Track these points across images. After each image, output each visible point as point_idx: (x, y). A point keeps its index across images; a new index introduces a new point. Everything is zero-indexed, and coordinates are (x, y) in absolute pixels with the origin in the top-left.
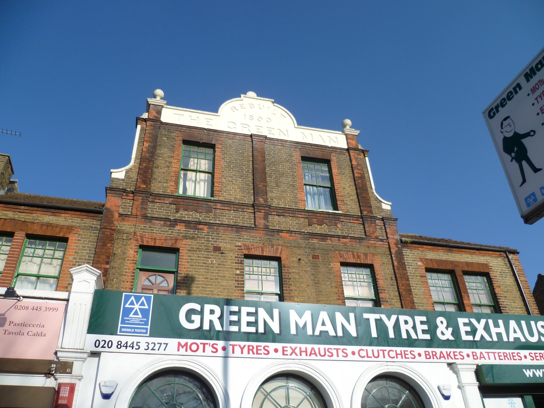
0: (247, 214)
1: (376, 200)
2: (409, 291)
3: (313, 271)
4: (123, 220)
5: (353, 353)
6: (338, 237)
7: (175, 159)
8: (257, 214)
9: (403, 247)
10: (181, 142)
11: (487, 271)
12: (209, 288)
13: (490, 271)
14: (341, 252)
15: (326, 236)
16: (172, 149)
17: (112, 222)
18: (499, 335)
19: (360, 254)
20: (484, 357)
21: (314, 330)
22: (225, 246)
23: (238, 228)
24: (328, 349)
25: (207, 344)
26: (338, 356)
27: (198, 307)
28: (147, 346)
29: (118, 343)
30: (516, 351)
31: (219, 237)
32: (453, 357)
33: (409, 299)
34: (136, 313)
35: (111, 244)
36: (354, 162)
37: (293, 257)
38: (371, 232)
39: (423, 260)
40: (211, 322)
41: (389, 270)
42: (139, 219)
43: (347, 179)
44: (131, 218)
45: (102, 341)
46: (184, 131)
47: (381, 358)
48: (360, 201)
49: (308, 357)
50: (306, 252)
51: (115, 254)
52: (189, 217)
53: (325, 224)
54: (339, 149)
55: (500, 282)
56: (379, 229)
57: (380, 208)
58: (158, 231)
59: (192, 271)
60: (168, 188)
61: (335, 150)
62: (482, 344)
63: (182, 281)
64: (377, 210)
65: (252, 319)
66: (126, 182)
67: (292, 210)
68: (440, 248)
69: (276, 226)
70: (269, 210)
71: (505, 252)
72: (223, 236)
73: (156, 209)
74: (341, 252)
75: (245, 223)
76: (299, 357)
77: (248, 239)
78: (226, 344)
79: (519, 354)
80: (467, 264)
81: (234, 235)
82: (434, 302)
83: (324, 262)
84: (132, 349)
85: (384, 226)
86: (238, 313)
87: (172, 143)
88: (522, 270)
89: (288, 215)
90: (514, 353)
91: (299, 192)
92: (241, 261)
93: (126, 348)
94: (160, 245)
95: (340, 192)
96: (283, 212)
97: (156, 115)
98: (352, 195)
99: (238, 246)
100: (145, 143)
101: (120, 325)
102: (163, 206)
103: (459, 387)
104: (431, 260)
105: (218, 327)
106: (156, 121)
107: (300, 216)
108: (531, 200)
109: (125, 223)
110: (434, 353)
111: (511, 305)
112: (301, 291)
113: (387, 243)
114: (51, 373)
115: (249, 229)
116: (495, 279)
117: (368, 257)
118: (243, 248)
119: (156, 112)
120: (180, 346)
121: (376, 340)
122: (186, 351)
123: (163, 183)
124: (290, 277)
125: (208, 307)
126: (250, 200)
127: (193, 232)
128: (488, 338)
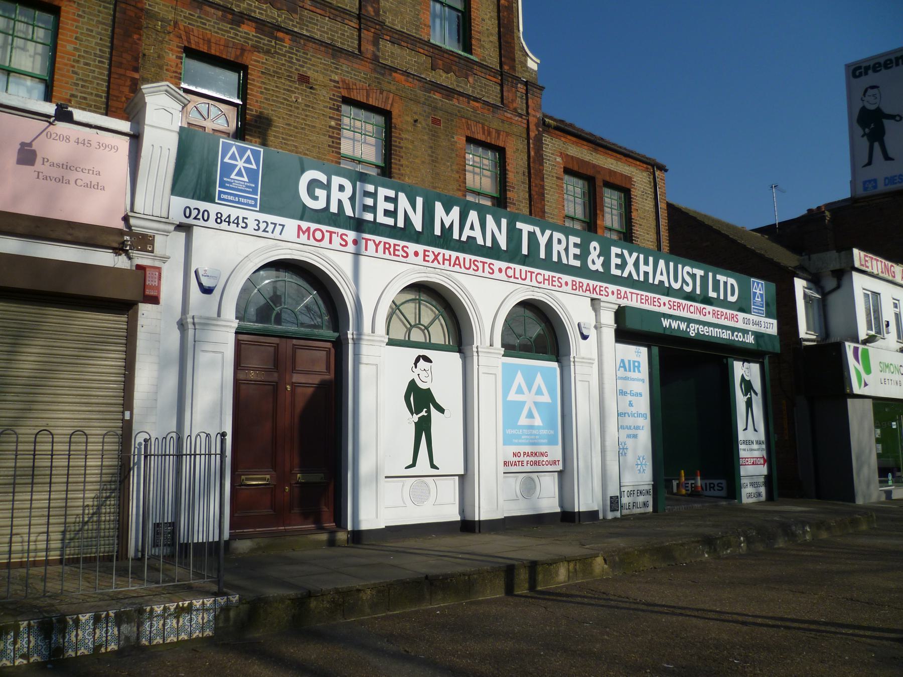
0: (348, 28)
1: (521, 51)
2: (542, 195)
3: (431, 141)
5: (500, 270)
6: (468, 97)
8: (364, 33)
9: (544, 131)
12: (293, 141)
15: (453, 93)
18: (646, 274)
20: (627, 298)
23: (335, 51)
24: (474, 261)
25: (335, 233)
26: (483, 272)
27: (323, 178)
28: (257, 225)
32: (598, 293)
34: (239, 174)
37: (407, 115)
38: (510, 100)
40: (340, 202)
43: (489, 5)
47: (528, 281)
49: (451, 268)
50: (425, 112)
52: (261, 14)
56: (519, 97)
57: (524, 64)
58: (214, 27)
59: (268, 110)
62: (629, 282)
63: (253, 123)
64: (520, 66)
68: (585, 143)
70: (382, 30)
71: (653, 166)
72: (313, 59)
75: (344, 44)
76: (441, 266)
77: (348, 72)
78: (358, 236)
79: (560, 280)
80: (611, 172)
81: (328, 61)
82: (566, 216)
83: (446, 131)
84: (237, 226)
85: (527, 94)
86: (374, 195)
88: (665, 193)
89: (405, 44)
90: (555, 277)
95: (477, 25)
96: (401, 38)
98: (492, 34)
99: (334, 81)
101: (218, 189)
105: (349, 212)
107: (422, 51)
108: (870, 186)
110: (581, 285)
111: (644, 236)
112: (414, 169)
113: (525, 121)
115: (350, 55)
117: (501, 137)
118: (340, 85)
120: (301, 232)
122: (309, 238)
124: (402, 145)
128: (635, 277)
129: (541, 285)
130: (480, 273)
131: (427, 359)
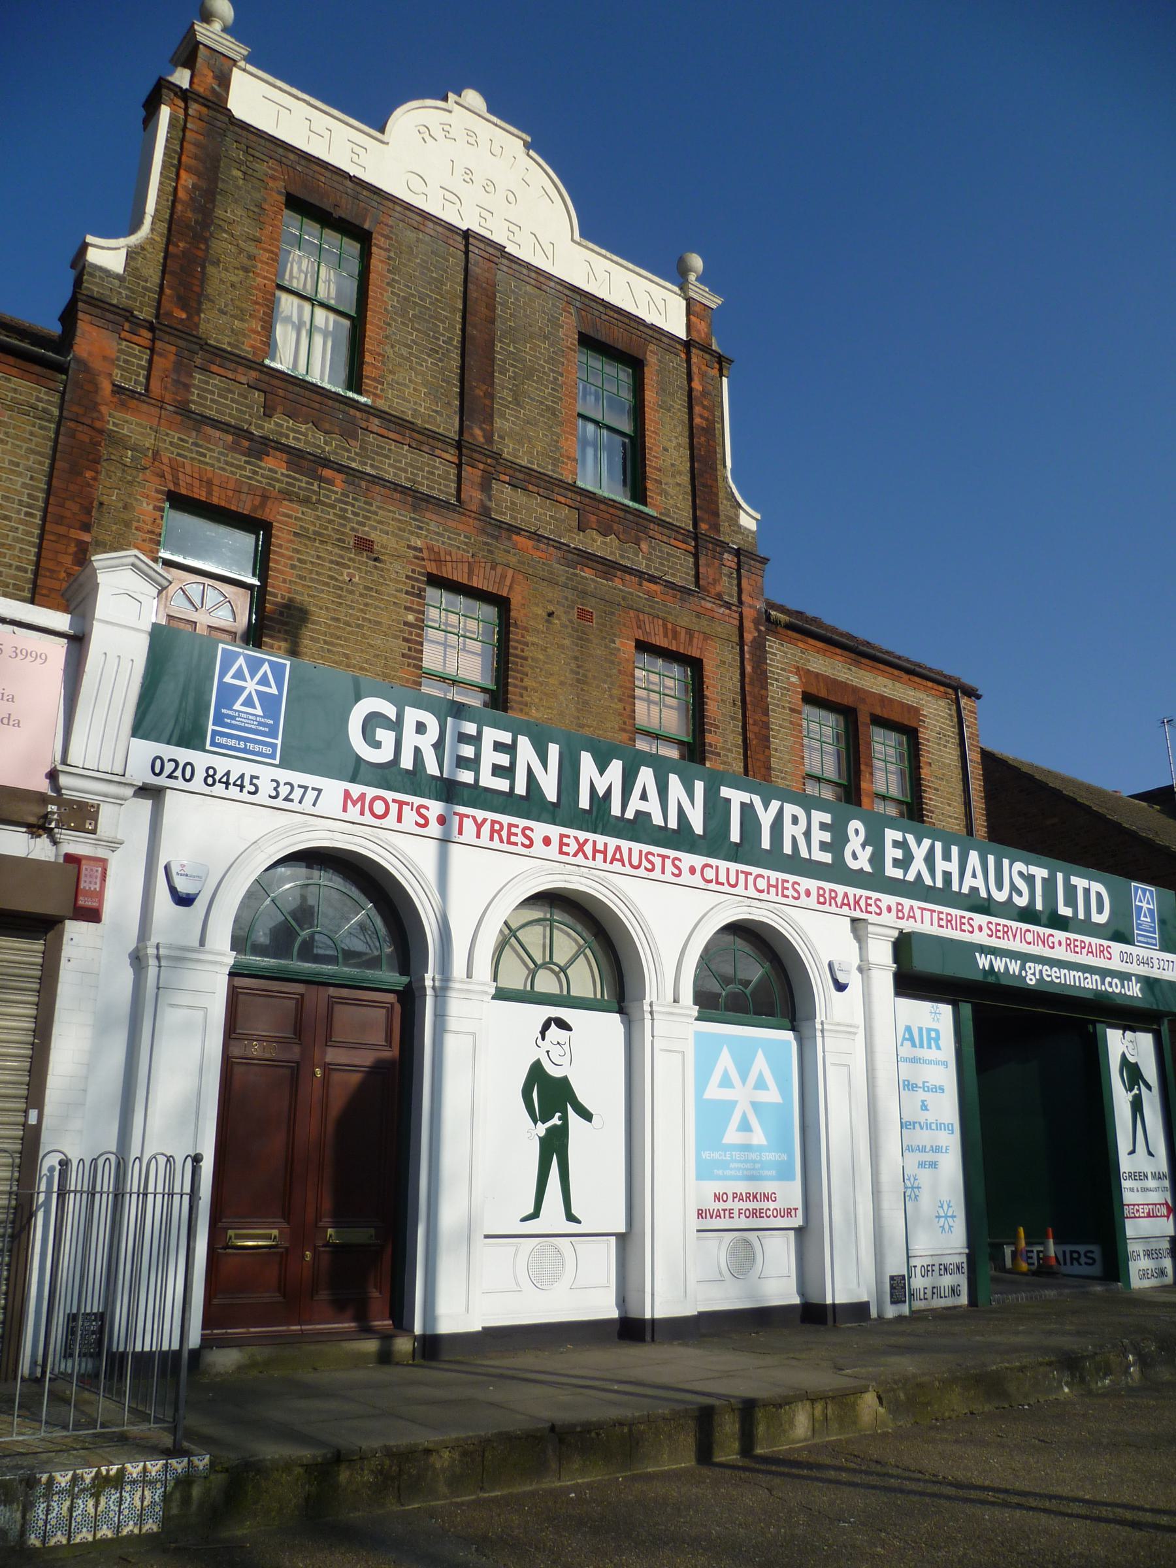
0: (440, 463)
2: (766, 740)
3: (576, 648)
4: (123, 405)
5: (692, 870)
6: (640, 574)
7: (265, 250)
8: (467, 471)
10: (283, 199)
11: (914, 725)
12: (342, 646)
13: (920, 726)
14: (641, 615)
15: (614, 568)
16: (258, 214)
17: (95, 407)
18: (947, 876)
19: (678, 629)
20: (914, 917)
21: (624, 806)
22: (385, 542)
23: (418, 500)
25: (407, 804)
26: (663, 872)
27: (390, 711)
28: (275, 789)
29: (207, 771)
30: (968, 914)
31: (369, 512)
32: (864, 909)
33: (760, 757)
35: (93, 474)
36: (697, 385)
37: (537, 605)
38: (710, 580)
39: (802, 673)
40: (417, 751)
41: (732, 681)
42: (168, 413)
43: (675, 425)
44: (145, 405)
45: (285, 784)
46: (289, 163)
47: (740, 889)
48: (698, 493)
49: (607, 866)
50: (566, 599)
51: (101, 504)
53: (613, 536)
54: (668, 337)
55: (933, 754)
56: (725, 574)
57: (734, 520)
58: (219, 460)
60: (244, 335)
61: (658, 336)
62: (916, 890)
63: (276, 616)
64: (727, 524)
65: (504, 760)
66: (128, 288)
67: (547, 478)
68: (838, 651)
69: (504, 514)
71: (955, 689)
72: (381, 512)
73: (213, 393)
74: (641, 615)
75: (433, 488)
76: (590, 863)
77: (437, 534)
78: (447, 810)
80: (883, 700)
81: (406, 515)
82: (807, 775)
83: (601, 631)
84: (241, 791)
86: (476, 740)
87: (257, 196)
88: (977, 736)
89: (535, 489)
91: (564, 431)
92: (420, 589)
93: (227, 788)
94: (223, 504)
97: (216, 87)
98: (680, 473)
99: (415, 549)
100: (183, 174)
102: (232, 388)
103: (860, 969)
104: (817, 675)
105: (432, 768)
106: (217, 104)
107: (562, 499)
109: (128, 417)
112: (546, 694)
113: (736, 615)
114: (47, 825)
115: (442, 507)
116: (926, 746)
117: (695, 640)
118: (425, 555)
119: (216, 77)
120: (349, 801)
121: (551, 808)
122: (362, 813)
123: (232, 316)
125: (413, 715)
126: (448, 425)
127: (307, 483)
128: (928, 881)
129: (764, 896)
130: (657, 874)
131: (563, 1025)
